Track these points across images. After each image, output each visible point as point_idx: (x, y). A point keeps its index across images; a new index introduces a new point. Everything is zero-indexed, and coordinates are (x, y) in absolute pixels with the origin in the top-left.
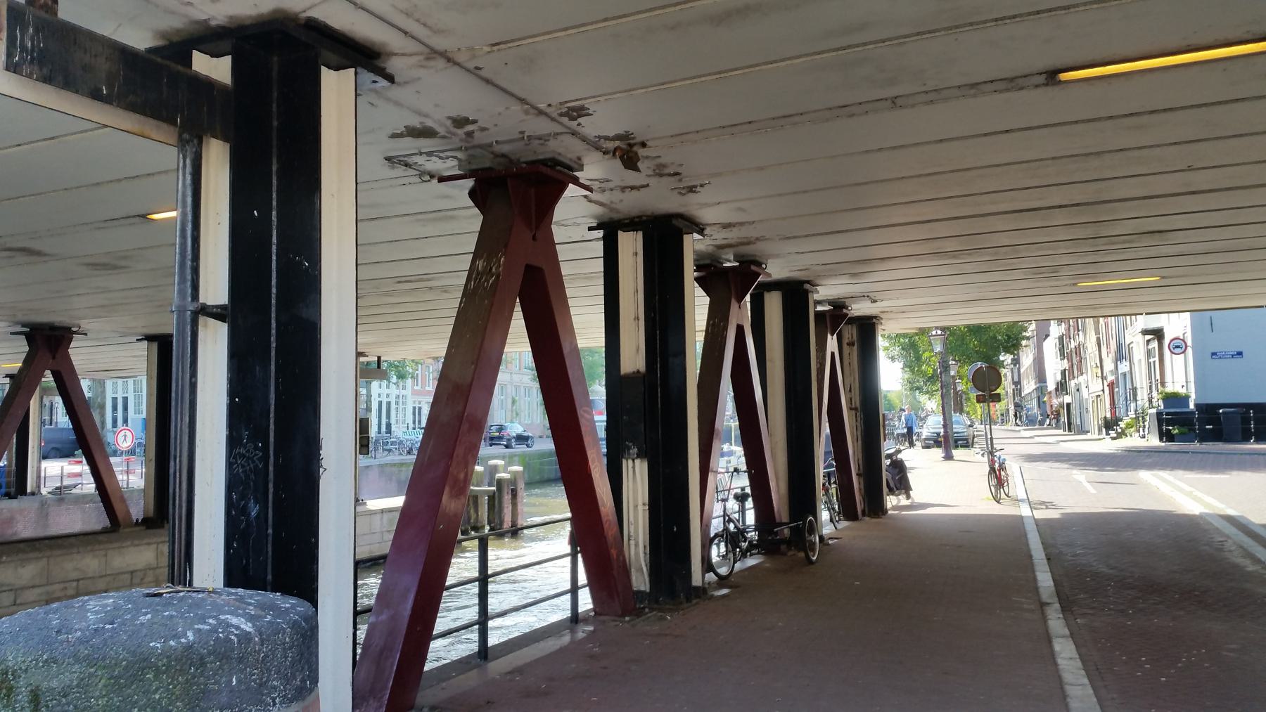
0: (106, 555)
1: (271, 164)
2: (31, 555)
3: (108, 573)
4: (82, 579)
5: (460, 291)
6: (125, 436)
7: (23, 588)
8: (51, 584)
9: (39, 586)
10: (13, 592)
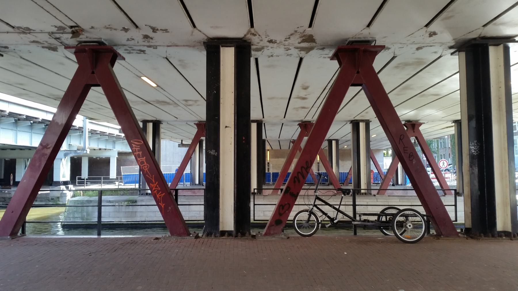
6: (443, 163)
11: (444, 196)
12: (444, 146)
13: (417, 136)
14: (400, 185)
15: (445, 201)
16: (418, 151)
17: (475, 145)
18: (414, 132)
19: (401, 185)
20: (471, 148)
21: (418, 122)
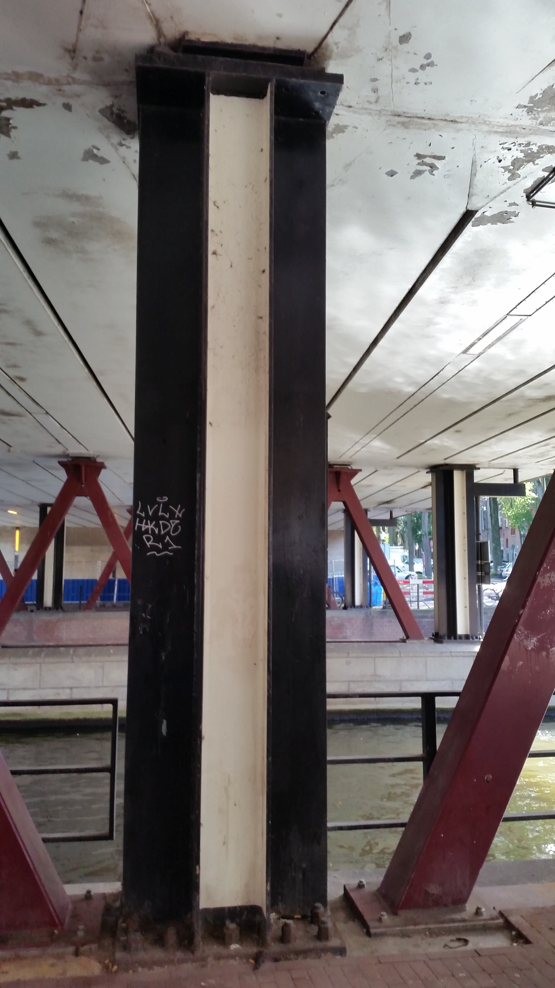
0: (103, 668)
1: (476, 601)
2: (23, 660)
3: (105, 684)
4: (75, 688)
5: (522, 787)
7: (15, 689)
8: (44, 688)
9: (30, 689)
10: (6, 691)
11: (403, 641)
12: (485, 527)
13: (345, 500)
14: (358, 607)
15: (402, 655)
16: (423, 535)
17: (160, 514)
18: (339, 491)
19: (361, 606)
20: (140, 528)
21: (348, 468)
